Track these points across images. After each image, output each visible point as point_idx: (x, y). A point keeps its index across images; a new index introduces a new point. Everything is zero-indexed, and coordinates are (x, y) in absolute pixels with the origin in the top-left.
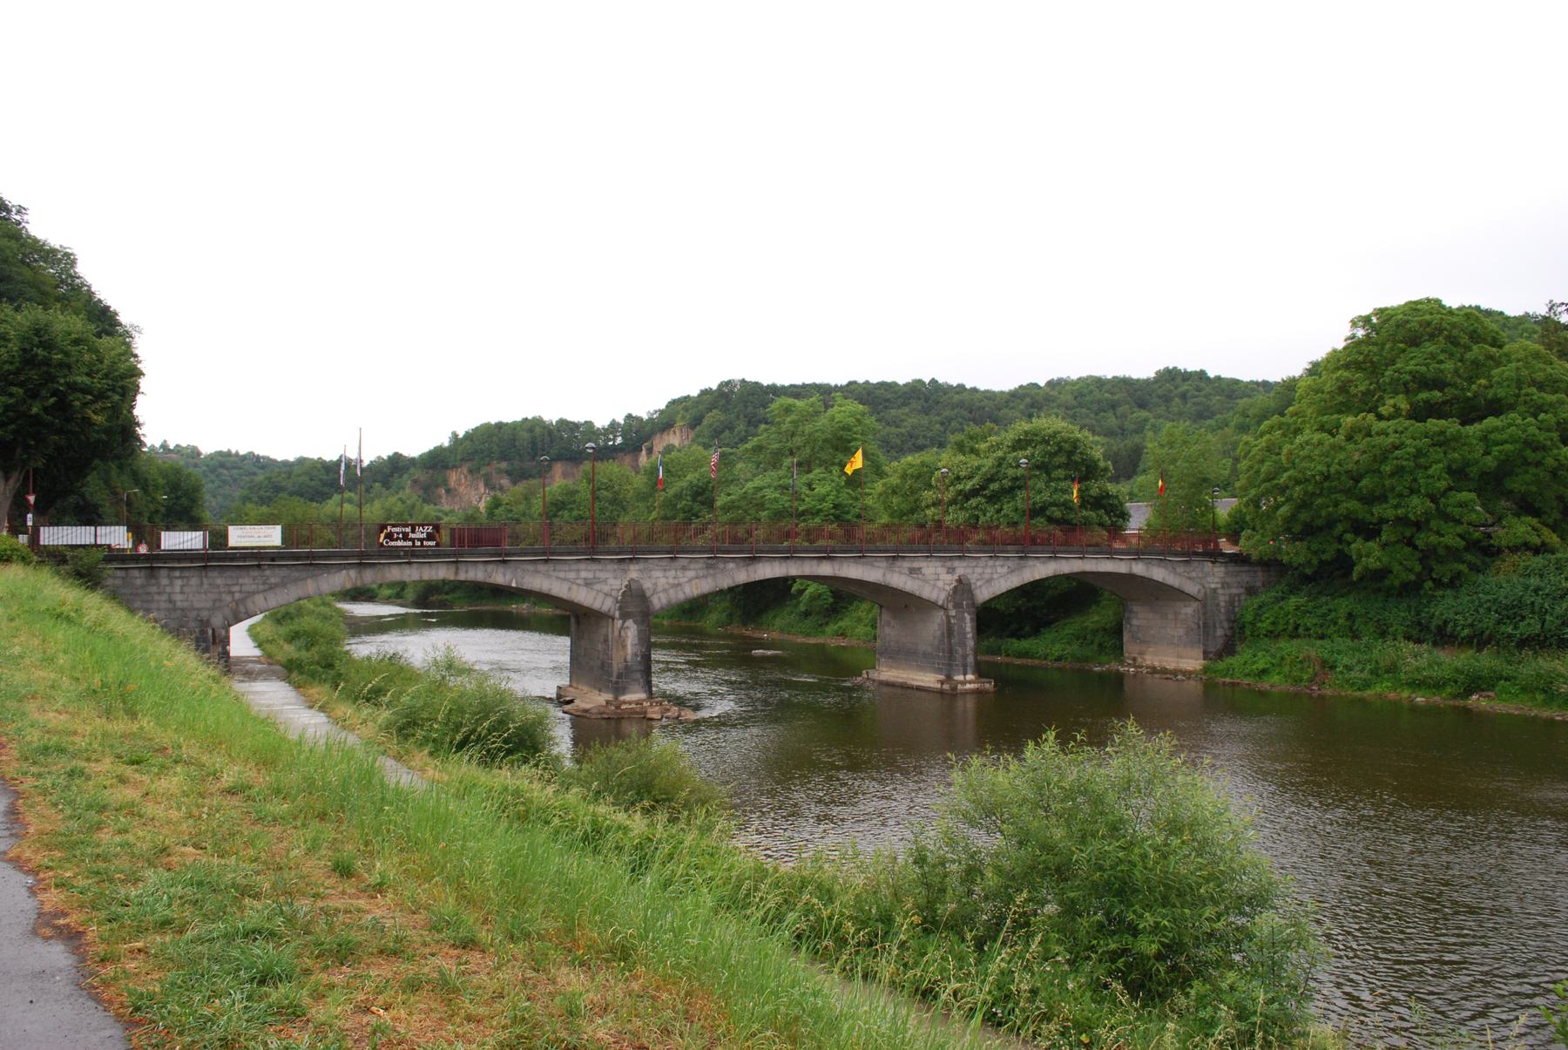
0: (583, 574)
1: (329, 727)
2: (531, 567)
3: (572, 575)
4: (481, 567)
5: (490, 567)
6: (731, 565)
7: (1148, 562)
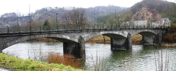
0: (73, 35)
1: (63, 58)
2: (63, 34)
3: (71, 35)
4: (54, 34)
5: (56, 34)
6: (96, 32)
7: (66, 35)
